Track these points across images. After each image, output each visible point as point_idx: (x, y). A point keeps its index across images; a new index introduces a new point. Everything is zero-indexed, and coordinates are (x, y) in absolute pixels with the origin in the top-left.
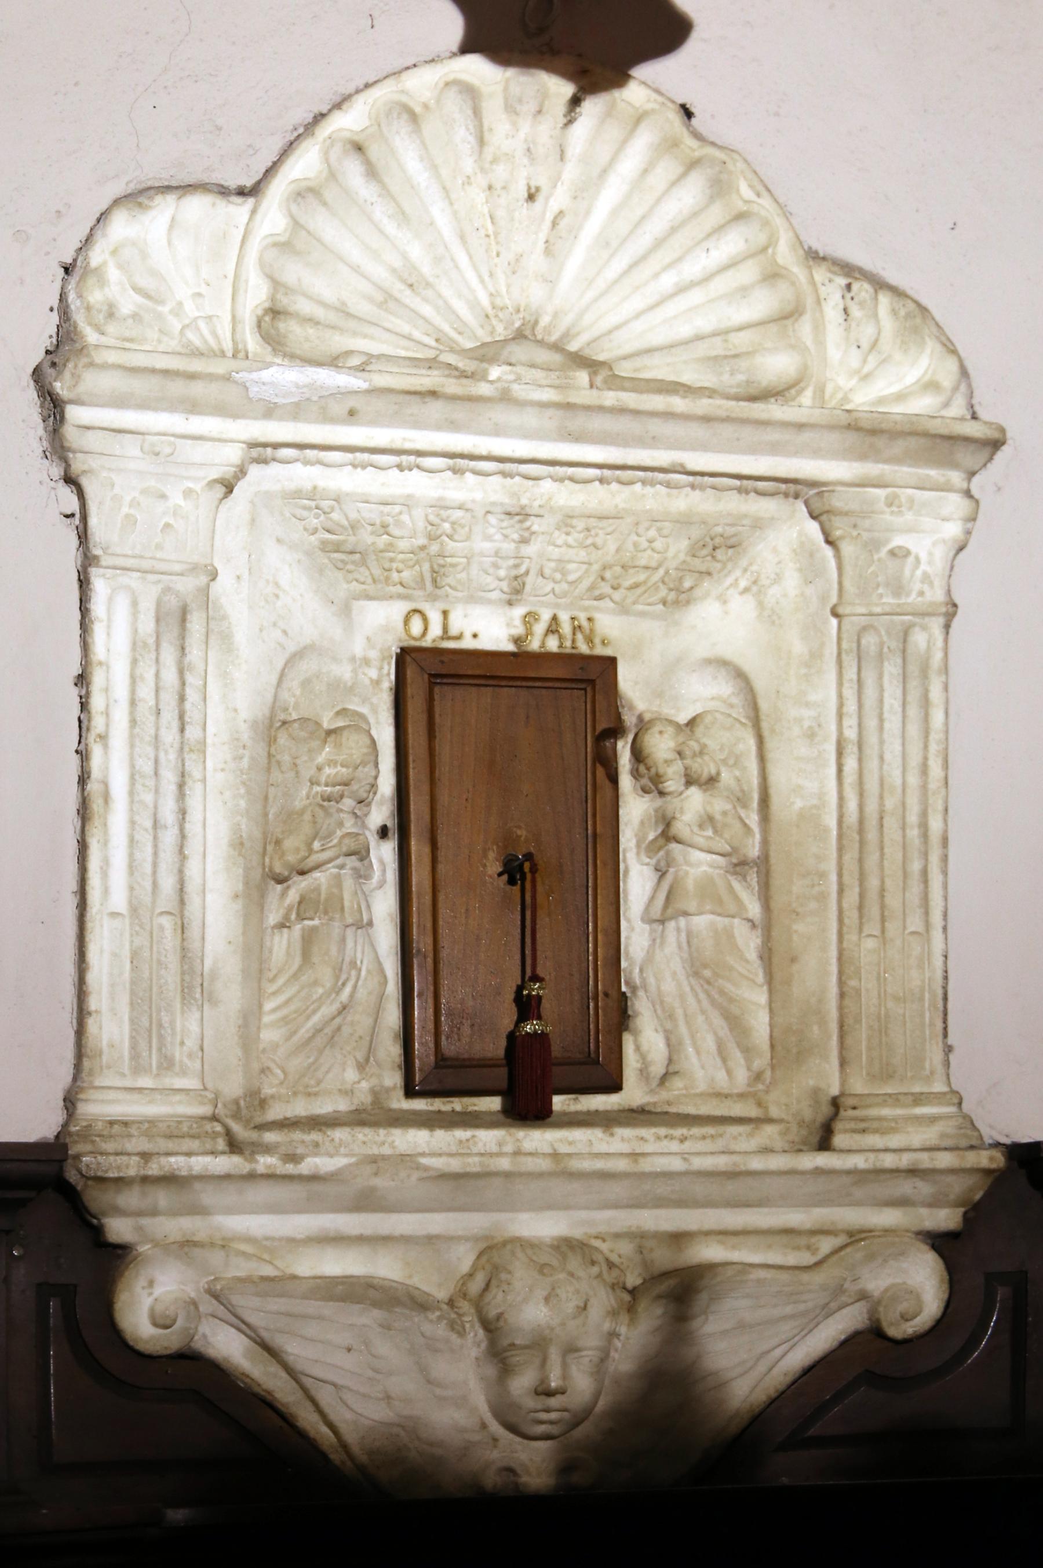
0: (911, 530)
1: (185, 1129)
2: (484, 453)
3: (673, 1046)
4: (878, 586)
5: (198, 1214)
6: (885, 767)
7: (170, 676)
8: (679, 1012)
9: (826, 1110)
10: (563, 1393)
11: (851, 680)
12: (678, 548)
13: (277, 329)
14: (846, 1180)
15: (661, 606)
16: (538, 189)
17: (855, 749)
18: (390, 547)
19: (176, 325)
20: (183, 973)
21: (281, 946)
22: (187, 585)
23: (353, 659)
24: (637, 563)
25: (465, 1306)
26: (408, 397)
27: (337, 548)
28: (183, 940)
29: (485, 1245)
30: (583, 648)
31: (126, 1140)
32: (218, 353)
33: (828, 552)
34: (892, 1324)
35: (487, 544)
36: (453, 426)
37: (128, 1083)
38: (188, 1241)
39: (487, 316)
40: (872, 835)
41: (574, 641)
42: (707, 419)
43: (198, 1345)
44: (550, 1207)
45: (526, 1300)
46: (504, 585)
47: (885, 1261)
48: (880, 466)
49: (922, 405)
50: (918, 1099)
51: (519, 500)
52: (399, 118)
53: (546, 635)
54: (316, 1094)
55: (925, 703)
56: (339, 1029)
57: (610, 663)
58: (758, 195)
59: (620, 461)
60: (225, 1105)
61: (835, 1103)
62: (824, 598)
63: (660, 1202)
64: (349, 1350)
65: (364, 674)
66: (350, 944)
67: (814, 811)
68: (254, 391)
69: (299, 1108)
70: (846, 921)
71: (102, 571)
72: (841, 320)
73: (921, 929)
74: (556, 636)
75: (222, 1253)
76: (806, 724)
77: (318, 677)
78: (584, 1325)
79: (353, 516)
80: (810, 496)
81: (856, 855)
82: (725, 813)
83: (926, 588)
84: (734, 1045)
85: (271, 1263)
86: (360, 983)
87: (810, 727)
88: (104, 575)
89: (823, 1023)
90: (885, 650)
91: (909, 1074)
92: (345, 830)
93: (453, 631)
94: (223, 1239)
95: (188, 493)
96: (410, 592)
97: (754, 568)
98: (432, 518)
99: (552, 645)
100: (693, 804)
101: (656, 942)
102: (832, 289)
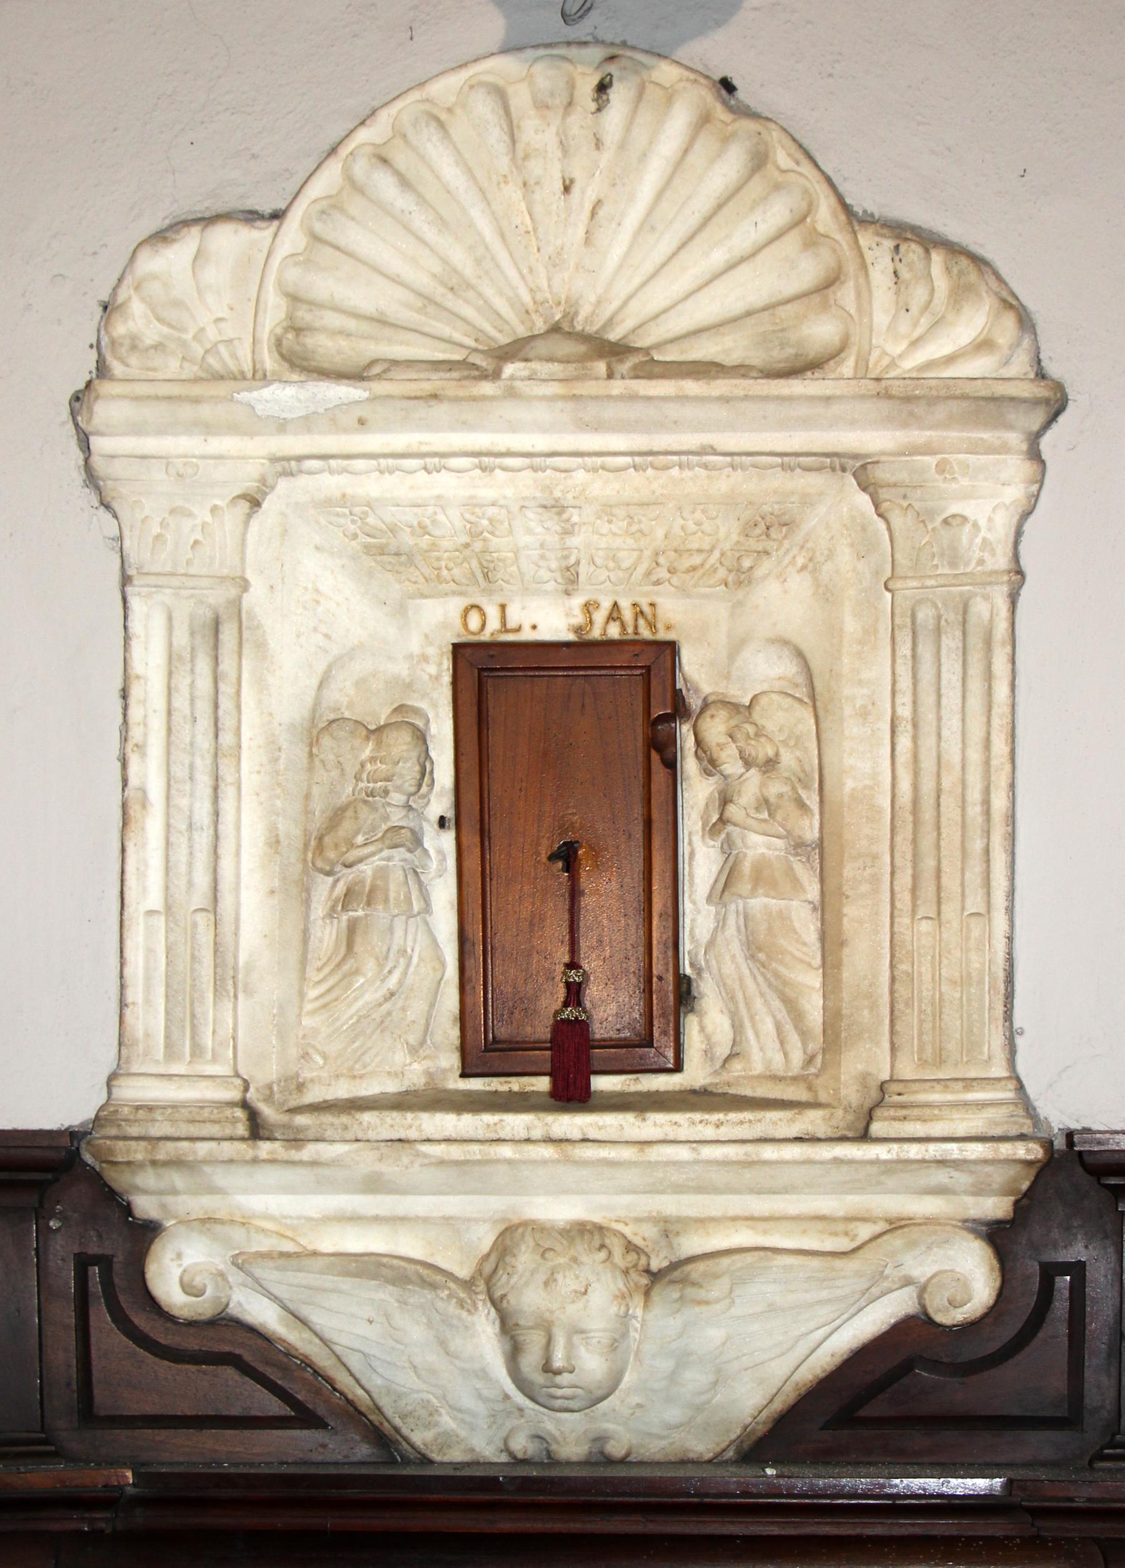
0: (968, 495)
1: (206, 1115)
2: (503, 450)
3: (737, 1028)
4: (933, 556)
5: (217, 1193)
6: (943, 744)
7: (204, 684)
8: (740, 996)
9: (874, 1094)
10: (571, 1372)
11: (905, 656)
12: (728, 531)
13: (304, 345)
14: (874, 1170)
15: (723, 587)
16: (572, 181)
17: (909, 727)
18: (434, 547)
19: (198, 350)
20: (216, 966)
21: (326, 936)
22: (218, 596)
23: (410, 657)
24: (689, 546)
25: (481, 1286)
26: (412, 403)
27: (382, 551)
28: (216, 935)
29: (503, 1227)
30: (646, 634)
31: (150, 1124)
32: (237, 373)
33: (881, 525)
34: (939, 1311)
35: (528, 539)
36: (466, 426)
37: (161, 1070)
38: (209, 1218)
39: (527, 312)
40: (928, 815)
41: (636, 627)
42: (725, 400)
43: (233, 1310)
44: (566, 1192)
45: (527, 1284)
46: (558, 575)
47: (929, 1248)
48: (928, 433)
49: (979, 366)
50: (969, 1083)
51: (551, 493)
52: (427, 126)
53: (607, 622)
54: (362, 1077)
55: (989, 676)
56: (389, 1013)
57: (671, 648)
58: (798, 163)
59: (644, 448)
60: (257, 1089)
61: (882, 1087)
62: (877, 573)
63: (679, 1189)
64: (371, 1322)
65: (422, 670)
66: (399, 932)
67: (867, 792)
68: (259, 408)
69: (342, 1090)
70: (898, 905)
71: (137, 589)
72: (891, 284)
73: (982, 909)
74: (618, 623)
75: (243, 1230)
76: (859, 703)
77: (374, 676)
78: (585, 1307)
79: (388, 519)
80: (862, 471)
81: (910, 837)
82: (780, 796)
83: (986, 556)
84: (792, 1028)
85: (292, 1240)
86: (412, 969)
87: (864, 707)
88: (139, 594)
89: (874, 1007)
90: (943, 623)
91: (965, 1059)
92: (390, 824)
93: (511, 625)
94: (243, 1217)
95: (214, 509)
96: (464, 588)
97: (810, 545)
98: (467, 516)
99: (614, 632)
100: (751, 785)
101: (721, 923)
102: (878, 251)
